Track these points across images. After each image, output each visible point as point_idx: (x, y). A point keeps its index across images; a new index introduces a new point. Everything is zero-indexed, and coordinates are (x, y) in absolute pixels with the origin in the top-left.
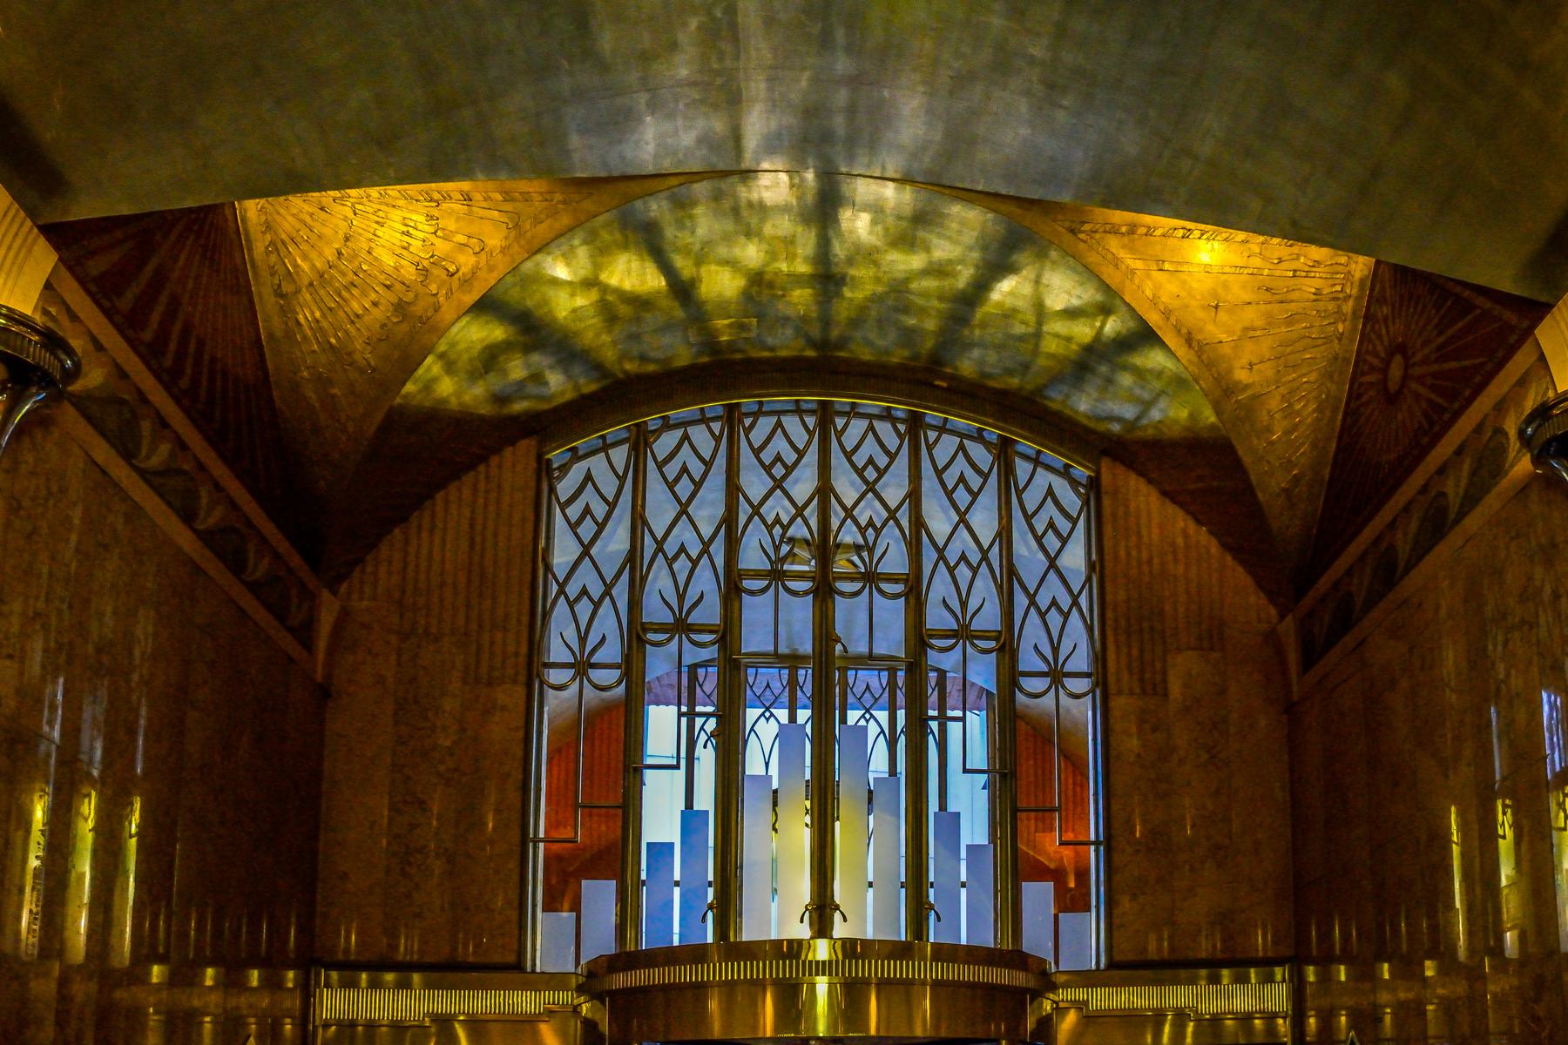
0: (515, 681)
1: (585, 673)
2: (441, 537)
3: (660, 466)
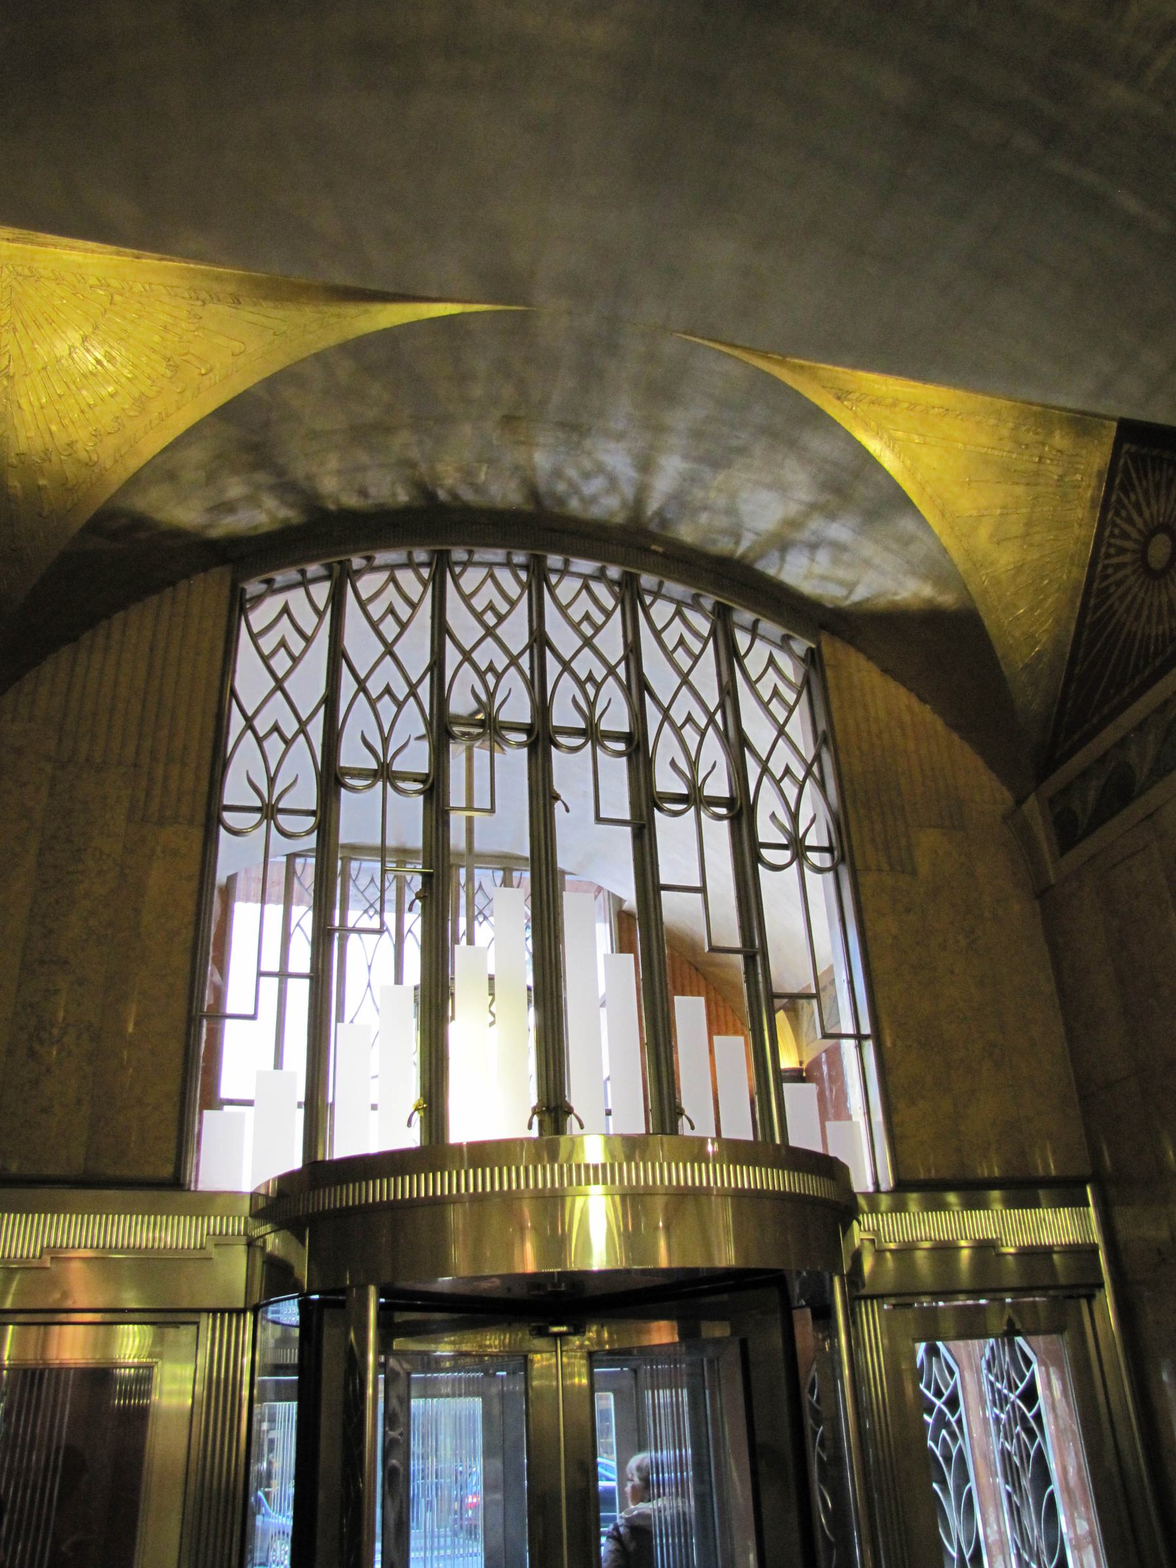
0: (191, 822)
1: (273, 818)
2: (118, 658)
3: (254, 637)
